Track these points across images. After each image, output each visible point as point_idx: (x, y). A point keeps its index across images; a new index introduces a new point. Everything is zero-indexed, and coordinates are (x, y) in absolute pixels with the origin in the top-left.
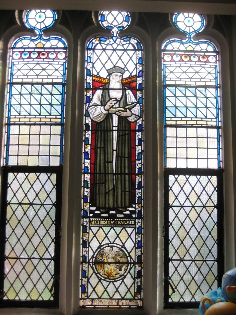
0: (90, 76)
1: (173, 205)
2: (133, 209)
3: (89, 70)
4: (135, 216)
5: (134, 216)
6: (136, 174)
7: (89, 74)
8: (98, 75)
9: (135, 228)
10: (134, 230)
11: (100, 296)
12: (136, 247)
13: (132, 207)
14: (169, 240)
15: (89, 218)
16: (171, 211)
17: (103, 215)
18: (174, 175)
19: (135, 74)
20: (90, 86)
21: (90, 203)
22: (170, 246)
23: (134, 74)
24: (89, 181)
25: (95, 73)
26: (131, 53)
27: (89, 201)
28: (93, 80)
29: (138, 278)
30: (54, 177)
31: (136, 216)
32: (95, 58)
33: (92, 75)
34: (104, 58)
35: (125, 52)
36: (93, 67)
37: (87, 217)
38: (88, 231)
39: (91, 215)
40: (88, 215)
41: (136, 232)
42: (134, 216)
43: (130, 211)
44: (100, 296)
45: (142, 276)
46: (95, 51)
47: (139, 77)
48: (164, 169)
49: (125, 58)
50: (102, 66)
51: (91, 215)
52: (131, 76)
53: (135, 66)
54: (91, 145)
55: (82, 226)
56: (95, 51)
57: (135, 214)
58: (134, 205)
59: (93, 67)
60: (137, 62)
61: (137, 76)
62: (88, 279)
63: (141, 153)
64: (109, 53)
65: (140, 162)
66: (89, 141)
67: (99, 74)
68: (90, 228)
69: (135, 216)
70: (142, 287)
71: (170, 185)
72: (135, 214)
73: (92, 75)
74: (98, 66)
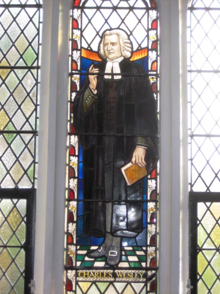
0: (77, 50)
1: (203, 248)
2: (142, 253)
3: (75, 20)
4: (146, 265)
5: (144, 264)
6: (147, 201)
7: (75, 48)
8: (89, 48)
9: (146, 285)
10: (145, 288)
11: (94, 285)
12: (150, 48)
13: (142, 250)
14: (198, 274)
15: (76, 269)
16: (200, 256)
17: (97, 264)
18: (205, 202)
19: (146, 46)
20: (77, 65)
21: (76, 245)
22: (200, 229)
23: (144, 45)
24: (75, 167)
25: (85, 45)
26: (140, 13)
27: (75, 242)
28: (81, 58)
29: (152, 29)
30: (23, 203)
31: (148, 266)
32: (85, 21)
33: (79, 48)
34: (98, 21)
35: (131, 12)
36: (82, 36)
37: (72, 268)
38: (74, 289)
39: (79, 264)
40: (74, 265)
41: (148, 289)
42: (144, 264)
43: (138, 256)
44: (94, 285)
45: (158, 113)
46: (85, 10)
47: (152, 50)
48: (190, 192)
49: (131, 20)
50: (121, 21)
51: (79, 264)
52: (140, 48)
53: (146, 34)
54: (77, 178)
55: (71, 42)
56: (85, 10)
57: (146, 261)
58: (144, 248)
59: (82, 36)
60: (150, 27)
61: (150, 48)
62: (82, 32)
63: (156, 61)
64: (106, 13)
65: (154, 53)
66: (73, 238)
67: (91, 46)
68: (77, 283)
69: (146, 265)
70: (158, 192)
71: (199, 217)
72: (146, 261)
73: (79, 48)
74: (89, 34)
